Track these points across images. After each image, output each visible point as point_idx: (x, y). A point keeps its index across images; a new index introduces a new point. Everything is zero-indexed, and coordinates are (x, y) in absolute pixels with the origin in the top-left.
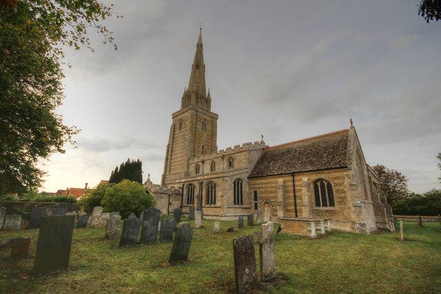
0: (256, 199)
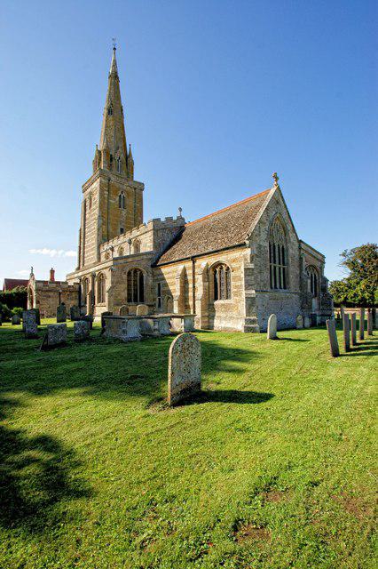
0: (159, 295)
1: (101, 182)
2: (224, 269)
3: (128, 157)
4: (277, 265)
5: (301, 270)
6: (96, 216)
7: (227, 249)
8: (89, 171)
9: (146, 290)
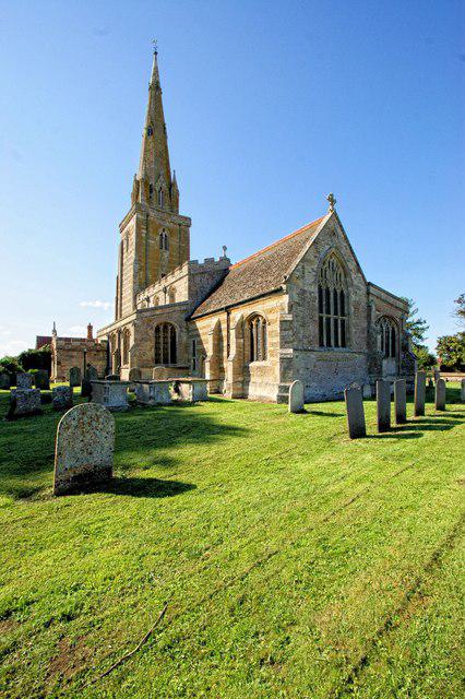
2: (261, 321)
3: (172, 186)
4: (332, 315)
5: (369, 323)
6: (132, 260)
7: (263, 296)
8: (127, 205)
9: (179, 349)
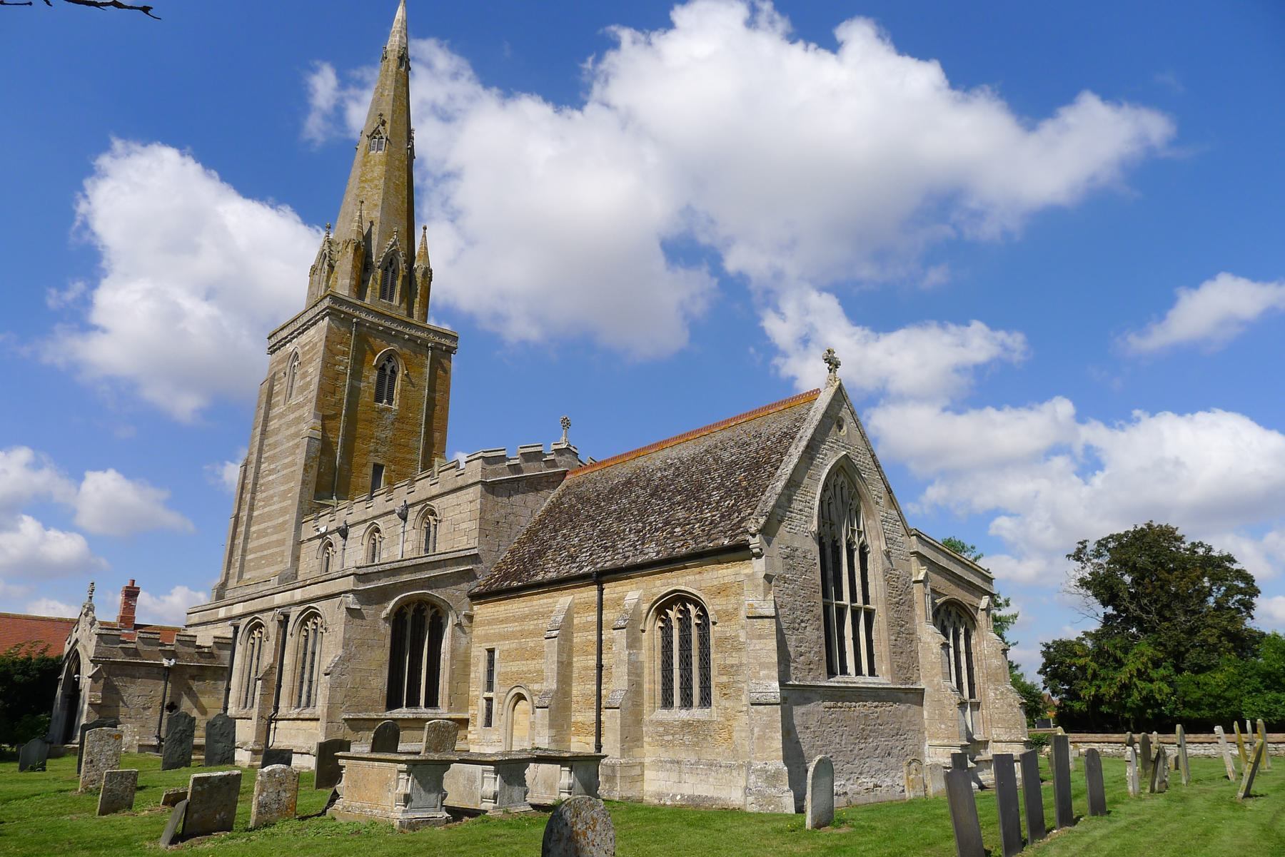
1: (329, 328)
